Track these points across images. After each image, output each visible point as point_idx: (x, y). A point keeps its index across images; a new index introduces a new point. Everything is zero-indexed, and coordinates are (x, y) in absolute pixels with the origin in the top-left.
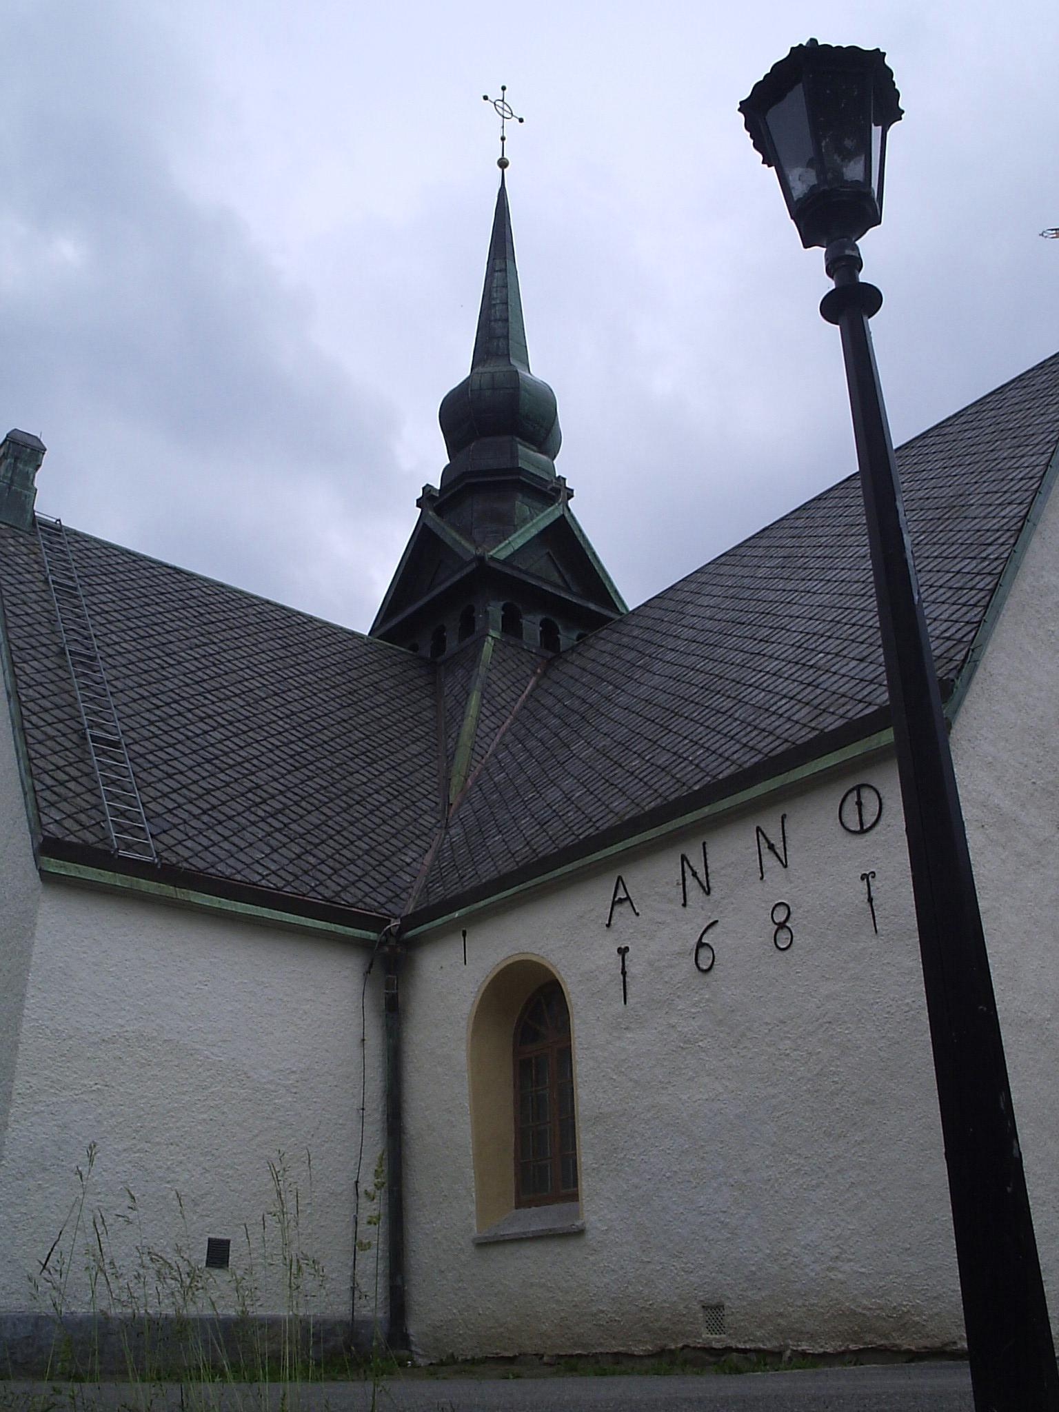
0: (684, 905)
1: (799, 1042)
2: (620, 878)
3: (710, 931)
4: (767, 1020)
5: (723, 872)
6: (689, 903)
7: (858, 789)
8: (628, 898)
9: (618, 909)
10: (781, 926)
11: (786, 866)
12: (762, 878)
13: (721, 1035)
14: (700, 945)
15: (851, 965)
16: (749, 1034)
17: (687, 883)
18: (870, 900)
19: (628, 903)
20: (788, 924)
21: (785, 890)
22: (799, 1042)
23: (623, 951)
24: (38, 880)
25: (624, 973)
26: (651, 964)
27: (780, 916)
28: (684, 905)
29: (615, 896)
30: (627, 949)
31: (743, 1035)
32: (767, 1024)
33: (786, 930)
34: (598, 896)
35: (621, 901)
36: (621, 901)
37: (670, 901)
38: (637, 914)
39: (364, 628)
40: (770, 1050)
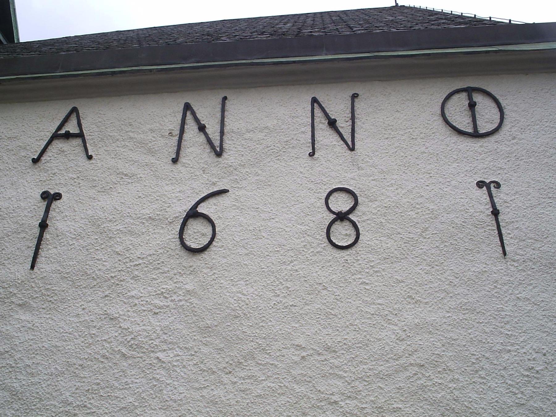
0: (175, 161)
1: (360, 386)
2: (74, 110)
3: (212, 201)
4: (301, 341)
5: (248, 136)
6: (182, 160)
7: (469, 91)
8: (81, 135)
9: (58, 144)
10: (341, 217)
11: (352, 149)
12: (312, 154)
13: (205, 350)
14: (193, 214)
15: (460, 290)
16: (261, 358)
17: (186, 136)
18: (495, 213)
19: (79, 141)
20: (351, 216)
21: (349, 175)
22: (360, 386)
23: (50, 198)
24: (197, 130)
25: (43, 226)
26: (94, 222)
27: (341, 204)
28: (175, 161)
29: (60, 128)
30: (58, 196)
31: (251, 356)
32: (299, 347)
33: (346, 224)
34: (41, 121)
35: (68, 136)
36: (68, 136)
37: (151, 152)
38: (90, 157)
39: (22, 40)
40: (300, 389)
